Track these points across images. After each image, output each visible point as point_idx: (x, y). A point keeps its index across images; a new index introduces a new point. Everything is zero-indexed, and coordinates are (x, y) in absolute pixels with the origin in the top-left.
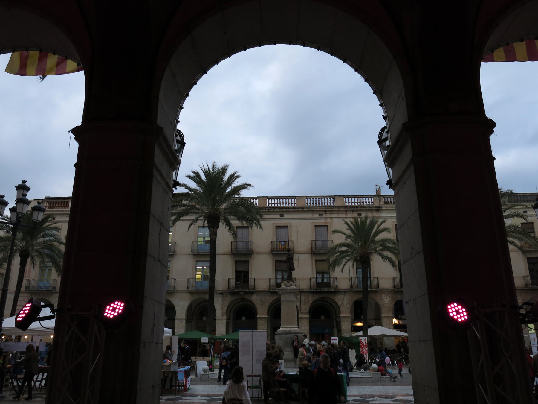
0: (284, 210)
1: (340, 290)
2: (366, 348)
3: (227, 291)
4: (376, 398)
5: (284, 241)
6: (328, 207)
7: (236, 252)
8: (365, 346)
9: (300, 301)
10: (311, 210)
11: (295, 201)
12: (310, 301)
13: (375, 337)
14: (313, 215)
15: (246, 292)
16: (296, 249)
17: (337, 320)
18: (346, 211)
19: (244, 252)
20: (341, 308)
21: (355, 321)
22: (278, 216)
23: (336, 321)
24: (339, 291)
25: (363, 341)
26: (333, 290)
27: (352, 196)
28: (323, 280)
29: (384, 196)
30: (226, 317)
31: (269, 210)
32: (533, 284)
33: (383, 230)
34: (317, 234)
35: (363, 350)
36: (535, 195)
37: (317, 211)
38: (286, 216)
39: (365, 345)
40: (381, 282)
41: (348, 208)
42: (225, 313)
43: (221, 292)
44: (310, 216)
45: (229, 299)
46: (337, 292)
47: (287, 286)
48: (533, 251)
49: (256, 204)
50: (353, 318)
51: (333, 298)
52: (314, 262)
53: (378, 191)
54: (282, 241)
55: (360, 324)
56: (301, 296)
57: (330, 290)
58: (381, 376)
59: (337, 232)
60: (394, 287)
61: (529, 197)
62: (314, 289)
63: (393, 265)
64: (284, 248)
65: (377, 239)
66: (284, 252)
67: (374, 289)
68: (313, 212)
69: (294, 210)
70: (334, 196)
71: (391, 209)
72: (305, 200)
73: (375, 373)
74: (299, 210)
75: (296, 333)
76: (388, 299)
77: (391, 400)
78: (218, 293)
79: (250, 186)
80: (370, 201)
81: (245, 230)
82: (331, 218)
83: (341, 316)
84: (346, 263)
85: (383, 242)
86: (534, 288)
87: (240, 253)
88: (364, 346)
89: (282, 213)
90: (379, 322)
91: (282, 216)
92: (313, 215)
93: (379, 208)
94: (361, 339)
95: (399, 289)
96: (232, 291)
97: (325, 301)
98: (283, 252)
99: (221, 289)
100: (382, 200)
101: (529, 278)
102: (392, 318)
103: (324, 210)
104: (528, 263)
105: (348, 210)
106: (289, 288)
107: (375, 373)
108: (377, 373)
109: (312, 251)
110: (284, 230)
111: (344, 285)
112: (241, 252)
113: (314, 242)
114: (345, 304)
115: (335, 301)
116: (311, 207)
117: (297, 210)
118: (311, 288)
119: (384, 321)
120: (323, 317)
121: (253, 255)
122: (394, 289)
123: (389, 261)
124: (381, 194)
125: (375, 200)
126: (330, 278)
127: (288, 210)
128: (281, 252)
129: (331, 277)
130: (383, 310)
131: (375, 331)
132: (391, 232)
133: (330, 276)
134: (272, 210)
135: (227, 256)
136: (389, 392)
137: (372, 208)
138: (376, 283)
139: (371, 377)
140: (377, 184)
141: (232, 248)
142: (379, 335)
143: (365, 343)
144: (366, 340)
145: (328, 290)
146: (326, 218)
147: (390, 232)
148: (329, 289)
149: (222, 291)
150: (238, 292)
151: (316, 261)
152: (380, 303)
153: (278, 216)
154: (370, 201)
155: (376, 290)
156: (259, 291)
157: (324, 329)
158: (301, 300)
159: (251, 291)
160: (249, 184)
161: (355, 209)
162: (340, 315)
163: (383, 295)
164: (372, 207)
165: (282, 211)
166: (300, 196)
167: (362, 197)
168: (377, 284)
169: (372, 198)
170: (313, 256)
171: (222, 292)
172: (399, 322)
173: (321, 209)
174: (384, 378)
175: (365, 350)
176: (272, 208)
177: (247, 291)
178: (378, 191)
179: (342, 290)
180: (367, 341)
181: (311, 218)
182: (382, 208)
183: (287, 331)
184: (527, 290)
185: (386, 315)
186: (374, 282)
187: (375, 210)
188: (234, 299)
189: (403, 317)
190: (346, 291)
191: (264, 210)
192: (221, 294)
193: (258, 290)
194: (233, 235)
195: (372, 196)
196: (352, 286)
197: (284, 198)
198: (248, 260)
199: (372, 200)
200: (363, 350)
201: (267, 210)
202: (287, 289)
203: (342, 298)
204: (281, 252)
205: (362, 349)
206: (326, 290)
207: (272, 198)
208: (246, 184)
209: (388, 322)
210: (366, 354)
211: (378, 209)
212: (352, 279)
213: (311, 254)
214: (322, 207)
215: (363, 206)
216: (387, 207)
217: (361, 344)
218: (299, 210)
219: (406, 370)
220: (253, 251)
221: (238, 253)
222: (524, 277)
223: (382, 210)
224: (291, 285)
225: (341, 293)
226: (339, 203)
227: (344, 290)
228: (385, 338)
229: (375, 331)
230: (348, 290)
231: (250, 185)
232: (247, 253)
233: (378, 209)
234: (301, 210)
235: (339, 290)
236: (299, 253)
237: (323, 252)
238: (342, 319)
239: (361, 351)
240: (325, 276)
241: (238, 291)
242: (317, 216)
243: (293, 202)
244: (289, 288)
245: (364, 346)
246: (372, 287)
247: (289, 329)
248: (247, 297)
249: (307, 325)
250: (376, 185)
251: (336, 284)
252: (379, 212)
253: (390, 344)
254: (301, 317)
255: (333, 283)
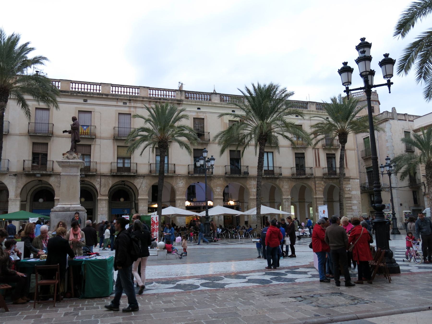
0: (88, 95)
1: (139, 174)
2: (157, 226)
3: (22, 172)
4: (154, 283)
5: (86, 126)
6: (132, 96)
7: (33, 134)
8: (156, 224)
9: (100, 184)
10: (116, 98)
11: (100, 88)
12: (110, 184)
13: (168, 216)
14: (117, 103)
15: (43, 174)
16: (98, 134)
17: (136, 202)
18: (150, 102)
19: (43, 134)
20: (139, 191)
21: (152, 203)
22: (81, 101)
23: (135, 203)
24: (139, 175)
25: (154, 219)
26: (133, 174)
27: (156, 88)
28: (124, 165)
29: (186, 92)
30: (20, 199)
31: (72, 94)
32: (297, 175)
33: (182, 117)
34: (120, 121)
35: (154, 227)
36: (305, 103)
37: (121, 99)
38: (89, 101)
39: (157, 223)
40: (177, 168)
41: (152, 99)
42: (19, 195)
43: (15, 173)
44: (114, 103)
45: (24, 181)
46: (136, 176)
47: (69, 159)
48: (300, 147)
49: (58, 87)
50: (151, 201)
51: (132, 181)
52: (116, 148)
53: (181, 87)
54: (84, 126)
55: (156, 206)
56: (101, 179)
57: (129, 174)
58: (168, 253)
59: (138, 117)
60: (189, 173)
61: (301, 104)
62: (114, 173)
63: (189, 151)
64: (86, 133)
65: (176, 124)
66: (86, 137)
67: (171, 174)
68: (117, 100)
69: (99, 96)
70: (139, 87)
71: (191, 103)
72: (110, 88)
73: (161, 251)
74: (104, 96)
75: (76, 210)
76: (182, 184)
77: (172, 286)
78: (12, 174)
79: (46, 59)
80: (173, 95)
81: (45, 112)
82: (135, 107)
83: (138, 198)
84: (145, 148)
85: (181, 128)
86: (298, 177)
87: (38, 135)
88: (155, 224)
89: (86, 98)
90: (173, 203)
91: (85, 101)
92: (117, 103)
93: (180, 101)
94: (153, 218)
95: (193, 175)
96: (27, 172)
97: (124, 185)
98: (84, 137)
99: (15, 171)
100: (183, 95)
101: (295, 169)
102: (185, 201)
103: (129, 98)
104: (296, 157)
105: (151, 101)
106: (71, 160)
107: (161, 251)
108: (163, 250)
109: (114, 137)
110: (87, 115)
111: (143, 170)
112: (39, 134)
113: (117, 129)
114: (144, 187)
115: (134, 184)
116: (116, 95)
117: (101, 96)
118: (111, 172)
119: (178, 203)
120: (122, 200)
121: (52, 138)
122: (188, 175)
123: (186, 147)
124: (183, 90)
125: (177, 94)
126: (130, 163)
127: (92, 95)
128: (83, 137)
129: (131, 162)
130: (177, 193)
131: (168, 211)
132: (189, 118)
133: (130, 161)
134: (75, 94)
135: (24, 137)
136: (172, 274)
137: (174, 101)
138: (173, 169)
139: (157, 255)
140: (180, 81)
141: (30, 129)
142: (172, 215)
143: (157, 221)
144: (158, 218)
145: (128, 174)
146: (130, 107)
147: (188, 119)
148: (129, 173)
149: (17, 172)
150: (34, 173)
151: (118, 146)
152: (175, 187)
153: (81, 101)
154: (173, 95)
155: (172, 175)
156: (57, 174)
157: (123, 210)
158: (101, 183)
159: (49, 173)
160: (44, 57)
161: (159, 101)
162: (138, 197)
163: (178, 180)
164: (175, 100)
165: (86, 96)
166: (106, 84)
167: (165, 91)
168: (174, 170)
169: (175, 92)
170: (115, 143)
171: (17, 173)
172: (191, 204)
173: (126, 98)
174: (171, 256)
175: (156, 227)
176: (75, 92)
177: (44, 173)
178: (181, 87)
179: (141, 174)
180: (158, 219)
181: (115, 106)
182: (182, 102)
183: (65, 208)
184: (293, 178)
185: (180, 198)
186: (171, 168)
187: (176, 103)
188: (30, 181)
189: (194, 200)
190: (145, 175)
191: (67, 94)
192: (15, 175)
193: (56, 173)
194: (27, 113)
195: (175, 91)
196: (151, 171)
197: (89, 83)
198: (47, 142)
199: (174, 94)
200: (154, 227)
201: (69, 94)
202: (69, 162)
203: (141, 182)
204: (83, 136)
205: (153, 227)
206: (126, 174)
207: (76, 82)
208: (41, 57)
209: (181, 204)
210: (157, 231)
211: (179, 102)
212: (152, 165)
213: (114, 140)
214: (126, 96)
215: (166, 98)
216: (187, 101)
217: (152, 222)
218: (104, 96)
219: (193, 245)
220: (52, 134)
221: (35, 135)
222: (291, 168)
223: (182, 103)
224: (74, 158)
225: (140, 178)
226: (143, 94)
227: (143, 175)
228: (178, 218)
229: (168, 211)
230: (147, 175)
231: (45, 58)
232: (46, 135)
233: (179, 102)
234: (106, 97)
235: (138, 174)
236: (101, 138)
237: (125, 138)
238: (140, 201)
239: (151, 228)
240: (126, 161)
241: (34, 173)
242: (121, 104)
243: (98, 89)
244: (71, 160)
245: (155, 224)
246: (169, 172)
247: (69, 206)
248: (45, 179)
249: (106, 207)
250: (179, 82)
251: (135, 169)
252: (180, 106)
253: (181, 223)
254: (100, 199)
255: (133, 167)
